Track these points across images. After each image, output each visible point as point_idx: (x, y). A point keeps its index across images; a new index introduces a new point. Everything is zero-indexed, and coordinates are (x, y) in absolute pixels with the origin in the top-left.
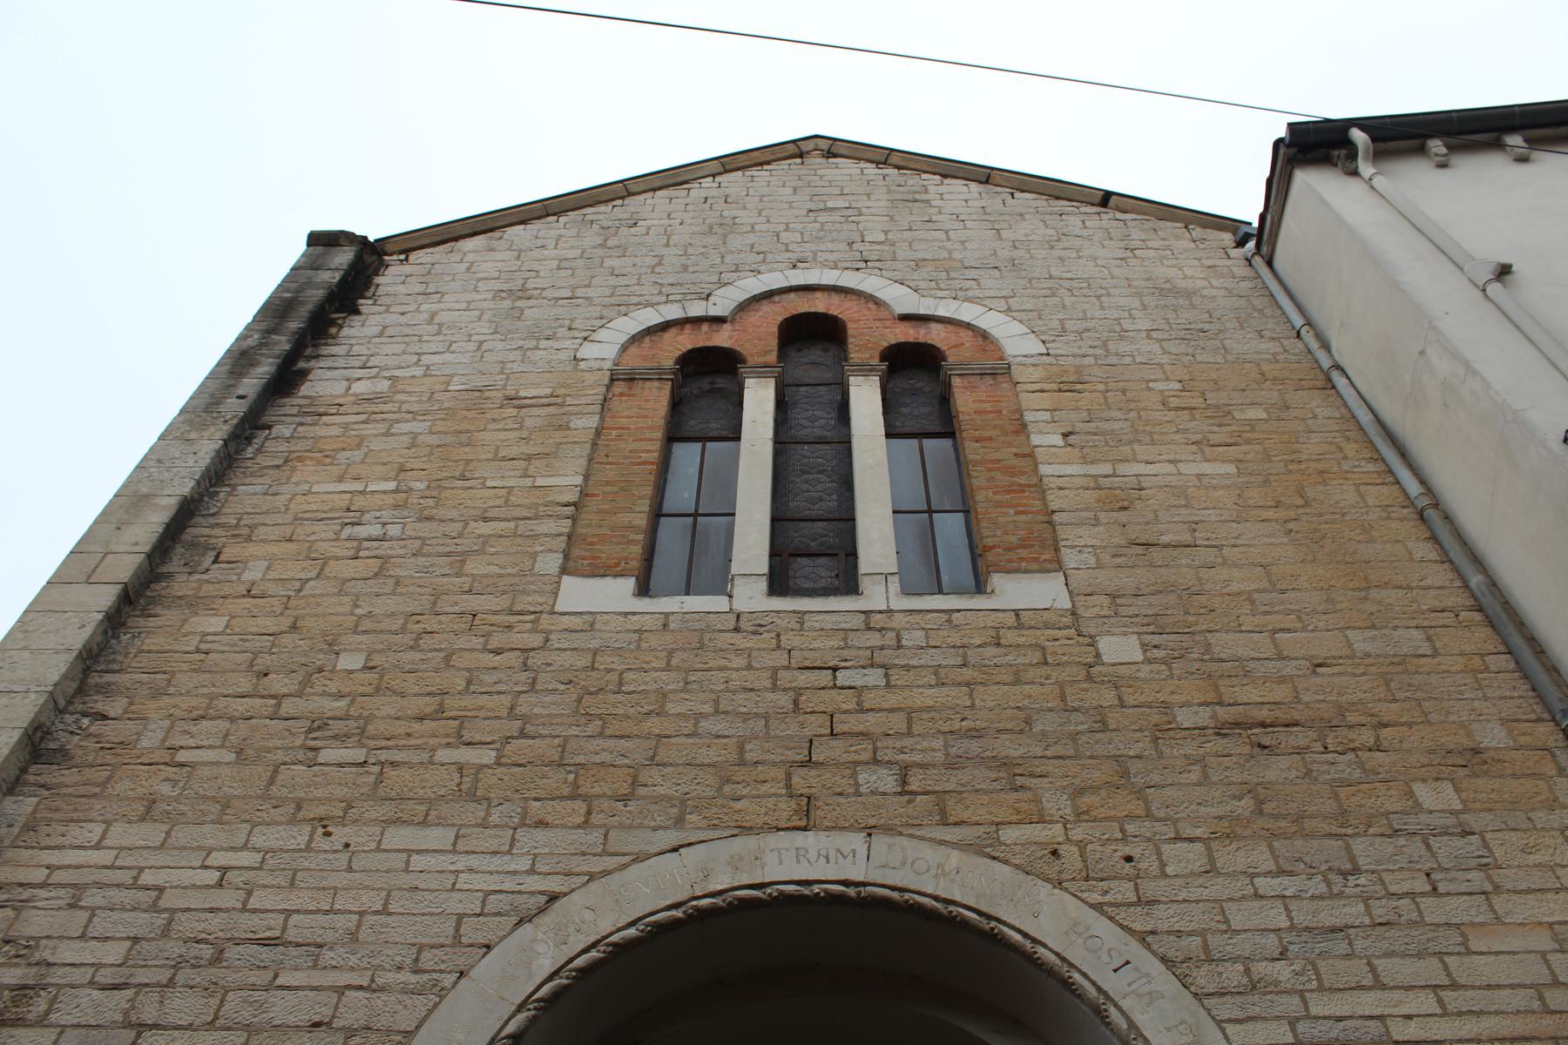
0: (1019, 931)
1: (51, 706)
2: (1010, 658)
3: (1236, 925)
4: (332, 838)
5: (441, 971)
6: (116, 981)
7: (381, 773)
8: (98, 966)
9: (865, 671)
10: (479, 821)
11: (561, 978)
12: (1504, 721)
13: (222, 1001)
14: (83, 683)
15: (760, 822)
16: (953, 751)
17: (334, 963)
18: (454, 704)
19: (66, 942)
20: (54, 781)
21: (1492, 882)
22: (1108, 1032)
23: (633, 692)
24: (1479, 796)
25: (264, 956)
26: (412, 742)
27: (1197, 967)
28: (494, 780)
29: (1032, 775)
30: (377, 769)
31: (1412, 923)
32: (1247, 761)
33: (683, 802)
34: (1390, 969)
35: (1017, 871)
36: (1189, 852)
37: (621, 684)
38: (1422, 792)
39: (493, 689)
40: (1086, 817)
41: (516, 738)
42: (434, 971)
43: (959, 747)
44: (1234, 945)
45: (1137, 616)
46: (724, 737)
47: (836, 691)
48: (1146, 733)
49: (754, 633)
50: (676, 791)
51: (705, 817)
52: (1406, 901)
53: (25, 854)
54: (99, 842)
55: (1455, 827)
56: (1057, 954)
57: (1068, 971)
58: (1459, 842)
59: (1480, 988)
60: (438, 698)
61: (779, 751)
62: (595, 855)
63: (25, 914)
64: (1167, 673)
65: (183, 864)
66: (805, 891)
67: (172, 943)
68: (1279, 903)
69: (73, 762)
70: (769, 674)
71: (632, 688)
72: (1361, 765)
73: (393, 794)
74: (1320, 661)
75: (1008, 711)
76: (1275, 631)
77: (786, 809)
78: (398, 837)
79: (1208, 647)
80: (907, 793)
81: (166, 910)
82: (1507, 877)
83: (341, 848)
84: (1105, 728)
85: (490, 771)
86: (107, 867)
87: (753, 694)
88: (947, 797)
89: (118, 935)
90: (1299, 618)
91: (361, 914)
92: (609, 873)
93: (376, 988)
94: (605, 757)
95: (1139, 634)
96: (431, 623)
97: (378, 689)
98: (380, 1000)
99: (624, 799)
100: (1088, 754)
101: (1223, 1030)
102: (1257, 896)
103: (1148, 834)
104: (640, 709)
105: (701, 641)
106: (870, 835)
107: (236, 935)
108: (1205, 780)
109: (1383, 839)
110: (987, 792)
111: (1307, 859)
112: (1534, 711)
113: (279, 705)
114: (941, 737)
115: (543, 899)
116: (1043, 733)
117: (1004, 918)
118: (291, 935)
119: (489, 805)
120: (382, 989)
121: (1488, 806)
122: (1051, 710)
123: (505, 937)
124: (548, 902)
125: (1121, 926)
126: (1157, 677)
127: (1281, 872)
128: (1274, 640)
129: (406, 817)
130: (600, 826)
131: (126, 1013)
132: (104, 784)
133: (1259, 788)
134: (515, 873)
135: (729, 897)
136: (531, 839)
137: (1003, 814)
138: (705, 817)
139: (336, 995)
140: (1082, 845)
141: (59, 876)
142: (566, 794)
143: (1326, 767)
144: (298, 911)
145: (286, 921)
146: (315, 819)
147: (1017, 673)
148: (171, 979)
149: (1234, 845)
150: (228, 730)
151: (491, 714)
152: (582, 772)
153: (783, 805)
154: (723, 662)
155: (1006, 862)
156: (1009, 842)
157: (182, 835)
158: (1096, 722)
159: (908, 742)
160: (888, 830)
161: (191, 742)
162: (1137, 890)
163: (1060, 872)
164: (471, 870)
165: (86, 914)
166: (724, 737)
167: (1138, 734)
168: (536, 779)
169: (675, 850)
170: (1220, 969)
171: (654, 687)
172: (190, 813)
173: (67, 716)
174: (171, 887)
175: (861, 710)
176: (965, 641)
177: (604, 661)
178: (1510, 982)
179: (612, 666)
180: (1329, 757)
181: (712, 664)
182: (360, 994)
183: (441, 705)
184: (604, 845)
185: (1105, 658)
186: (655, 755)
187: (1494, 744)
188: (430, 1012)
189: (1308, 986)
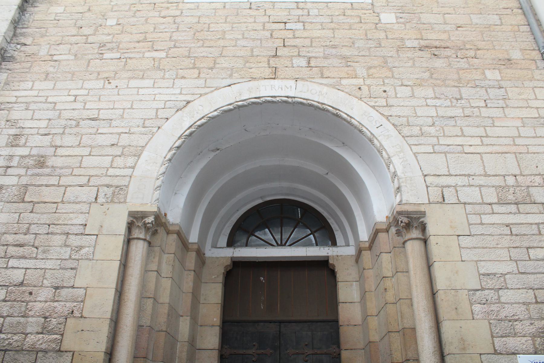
0: (346, 114)
1: (5, 41)
2: (348, 20)
3: (419, 114)
4: (112, 84)
5: (152, 127)
6: (46, 133)
7: (126, 61)
8: (39, 128)
9: (296, 24)
10: (162, 77)
12: (521, 50)
13: (81, 138)
14: (15, 32)
15: (259, 76)
16: (326, 53)
17: (116, 125)
18: (150, 37)
19: (27, 121)
20: (12, 67)
21: (506, 104)
22: (373, 147)
23: (214, 31)
24: (507, 75)
25: (93, 123)
26: (136, 50)
28: (166, 63)
29: (354, 62)
30: (125, 60)
31: (477, 116)
33: (232, 69)
34: (468, 131)
37: (209, 28)
38: (488, 73)
39: (164, 31)
40: (371, 77)
41: (173, 48)
42: (150, 127)
43: (329, 51)
45: (395, 6)
46: (246, 47)
47: (285, 31)
48: (395, 49)
49: (257, 10)
51: (240, 75)
52: (476, 109)
53: (7, 93)
54: (32, 88)
55: (497, 85)
56: (358, 122)
58: (497, 90)
59: (495, 137)
60: (144, 34)
61: (265, 52)
62: (202, 88)
63: (12, 112)
64: (404, 27)
65: (62, 94)
66: (274, 99)
67: (62, 120)
69: (17, 61)
70: (262, 24)
71: (213, 30)
72: (468, 63)
73: (131, 69)
74: (459, 25)
75: (347, 39)
76: (444, 14)
77: (268, 72)
78: (134, 83)
79: (420, 18)
80: (310, 67)
81: (58, 110)
82: (511, 103)
83: (115, 87)
84: (380, 46)
85: (164, 60)
86: (36, 96)
87: (256, 31)
88: (324, 68)
89: (44, 118)
90: (454, 9)
91: (124, 109)
92: (207, 94)
94: (204, 54)
95: (395, 13)
96: (139, 7)
97: (122, 32)
98: (132, 137)
99: (212, 69)
100: (374, 55)
101: (411, 148)
102: (427, 105)
103: (392, 83)
104: (216, 37)
105: (237, 13)
106: (296, 81)
107: (83, 117)
108: (413, 66)
109: (472, 88)
110: (337, 67)
111: (445, 94)
112: (533, 46)
113: (87, 38)
114: (322, 47)
115: (185, 103)
116: (358, 47)
117: (341, 110)
118: (101, 117)
120: (133, 133)
121: (510, 79)
122: (362, 39)
123: (173, 115)
124: (187, 103)
125: (380, 113)
126: (400, 29)
127: (436, 98)
128: (444, 17)
129: (136, 76)
130: (203, 78)
131: (51, 143)
132: (30, 68)
133: (432, 69)
134: (175, 94)
135: (248, 101)
136: (179, 83)
137: (343, 75)
138: (240, 75)
141: (20, 100)
143: (456, 63)
144: (102, 109)
145: (99, 112)
146: (104, 78)
147: (350, 26)
148: (64, 132)
149: (421, 88)
150: (70, 48)
151: (163, 40)
152: (196, 59)
154: (246, 20)
155: (343, 91)
156: (344, 84)
157: (59, 85)
158: (377, 44)
159: (311, 49)
160: (303, 79)
161: (58, 53)
162: (387, 102)
163: (361, 95)
164: (160, 94)
165: (32, 112)
166: (246, 47)
167: (392, 49)
168: (181, 62)
169: (229, 86)
170: (412, 128)
171: (221, 29)
172: (61, 77)
173: (12, 44)
174: (59, 102)
175: (295, 38)
176: (332, 13)
177: (203, 20)
178: (505, 136)
179: (206, 22)
180: (458, 60)
181: (241, 21)
182: (126, 135)
183: (145, 37)
185: (382, 21)
186: (222, 53)
187: (516, 58)
188: (150, 140)
189: (440, 135)
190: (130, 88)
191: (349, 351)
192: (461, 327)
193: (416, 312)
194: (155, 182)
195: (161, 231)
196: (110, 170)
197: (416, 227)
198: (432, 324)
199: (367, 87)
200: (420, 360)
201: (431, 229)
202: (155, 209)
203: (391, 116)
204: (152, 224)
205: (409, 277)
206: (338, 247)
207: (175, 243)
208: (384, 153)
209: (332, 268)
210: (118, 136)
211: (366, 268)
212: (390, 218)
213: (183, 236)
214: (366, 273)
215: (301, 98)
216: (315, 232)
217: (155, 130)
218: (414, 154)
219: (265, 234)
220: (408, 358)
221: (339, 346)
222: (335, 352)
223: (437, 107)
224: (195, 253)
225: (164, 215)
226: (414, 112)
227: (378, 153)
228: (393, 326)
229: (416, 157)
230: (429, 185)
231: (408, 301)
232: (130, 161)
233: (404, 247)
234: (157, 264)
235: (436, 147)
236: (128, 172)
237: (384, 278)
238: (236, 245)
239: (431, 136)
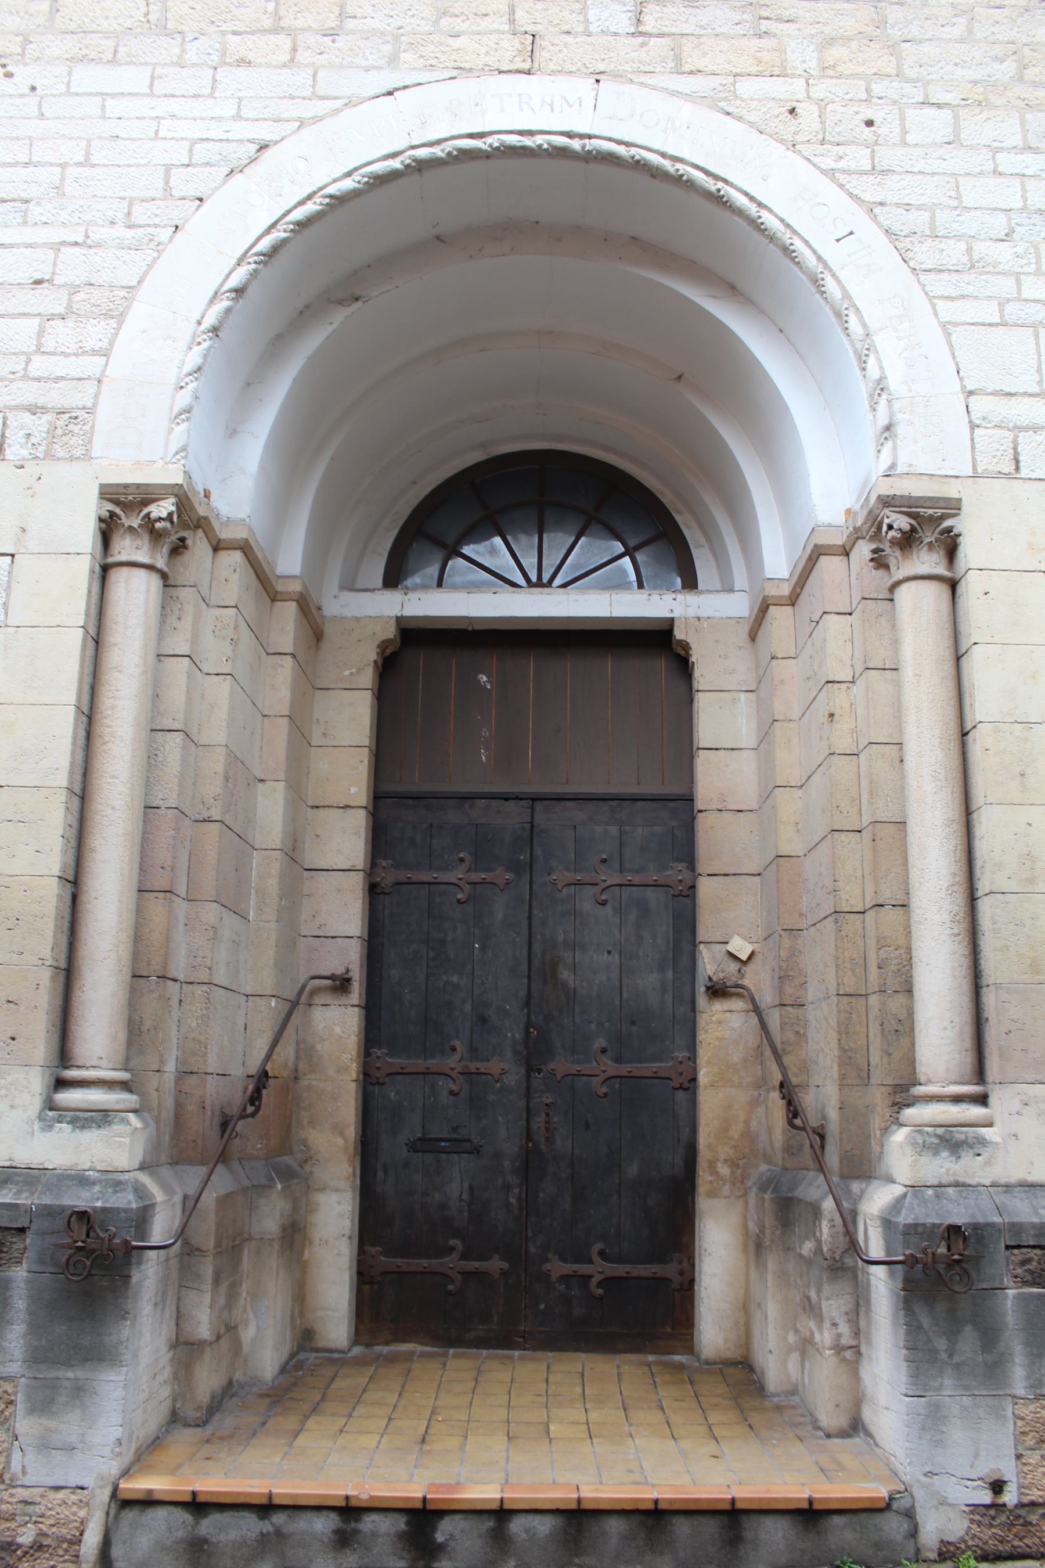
0: (746, 194)
3: (967, 202)
5: (156, 226)
10: (175, 59)
11: (279, 231)
17: (45, 220)
22: (822, 301)
27: (920, 242)
29: (779, 20)
32: (1021, 15)
33: (397, 38)
35: (751, 130)
36: (934, 119)
40: (831, 73)
42: (149, 225)
44: (961, 222)
50: (389, 25)
51: (422, 56)
56: (782, 220)
57: (791, 238)
62: (304, 98)
66: (527, 142)
68: (1016, 182)
73: (73, 26)
77: (508, 52)
78: (88, 78)
83: (27, 91)
88: (684, 40)
91: (63, 166)
92: (321, 119)
93: (92, 244)
99: (331, 34)
101: (934, 306)
103: (895, 97)
106: (598, 81)
110: (728, 37)
119: (184, 40)
123: (217, 189)
124: (258, 151)
125: (851, 195)
127: (1028, 148)
130: (307, 66)
133: (1026, 49)
134: (220, 119)
135: (449, 146)
136: (231, 79)
138: (422, 56)
139: (52, 252)
140: (822, 104)
142: (266, 27)
149: (984, 115)
153: (505, 44)
155: (740, 119)
156: (745, 97)
160: (618, 76)
162: (873, 158)
163: (795, 133)
169: (390, 93)
170: (942, 246)
182: (77, 250)
184: (314, 87)
188: (150, 267)
189: (1026, 269)
190: (77, 94)
191: (719, 877)
192: (1029, 824)
193: (912, 781)
194: (174, 396)
195: (199, 546)
196: (37, 360)
197: (930, 544)
198: (955, 812)
199: (815, 109)
200: (912, 905)
201: (970, 552)
202: (179, 479)
203: (881, 204)
204: (172, 522)
205: (898, 685)
206: (701, 592)
207: (236, 576)
208: (853, 320)
209: (683, 653)
210: (51, 254)
211: (780, 656)
212: (856, 514)
213: (260, 556)
214: (781, 669)
215: (610, 139)
216: (637, 548)
217: (165, 234)
218: (944, 326)
219: (493, 551)
220: (881, 901)
221: (692, 866)
222: (680, 881)
223: (1026, 179)
224: (294, 604)
225: (202, 493)
226: (953, 194)
227: (833, 319)
228: (845, 814)
229: (948, 335)
230: (978, 422)
231: (891, 751)
232: (96, 333)
233: (892, 600)
234: (189, 636)
235: (1009, 308)
236: (93, 365)
237: (830, 685)
238: (409, 582)
239: (998, 273)
